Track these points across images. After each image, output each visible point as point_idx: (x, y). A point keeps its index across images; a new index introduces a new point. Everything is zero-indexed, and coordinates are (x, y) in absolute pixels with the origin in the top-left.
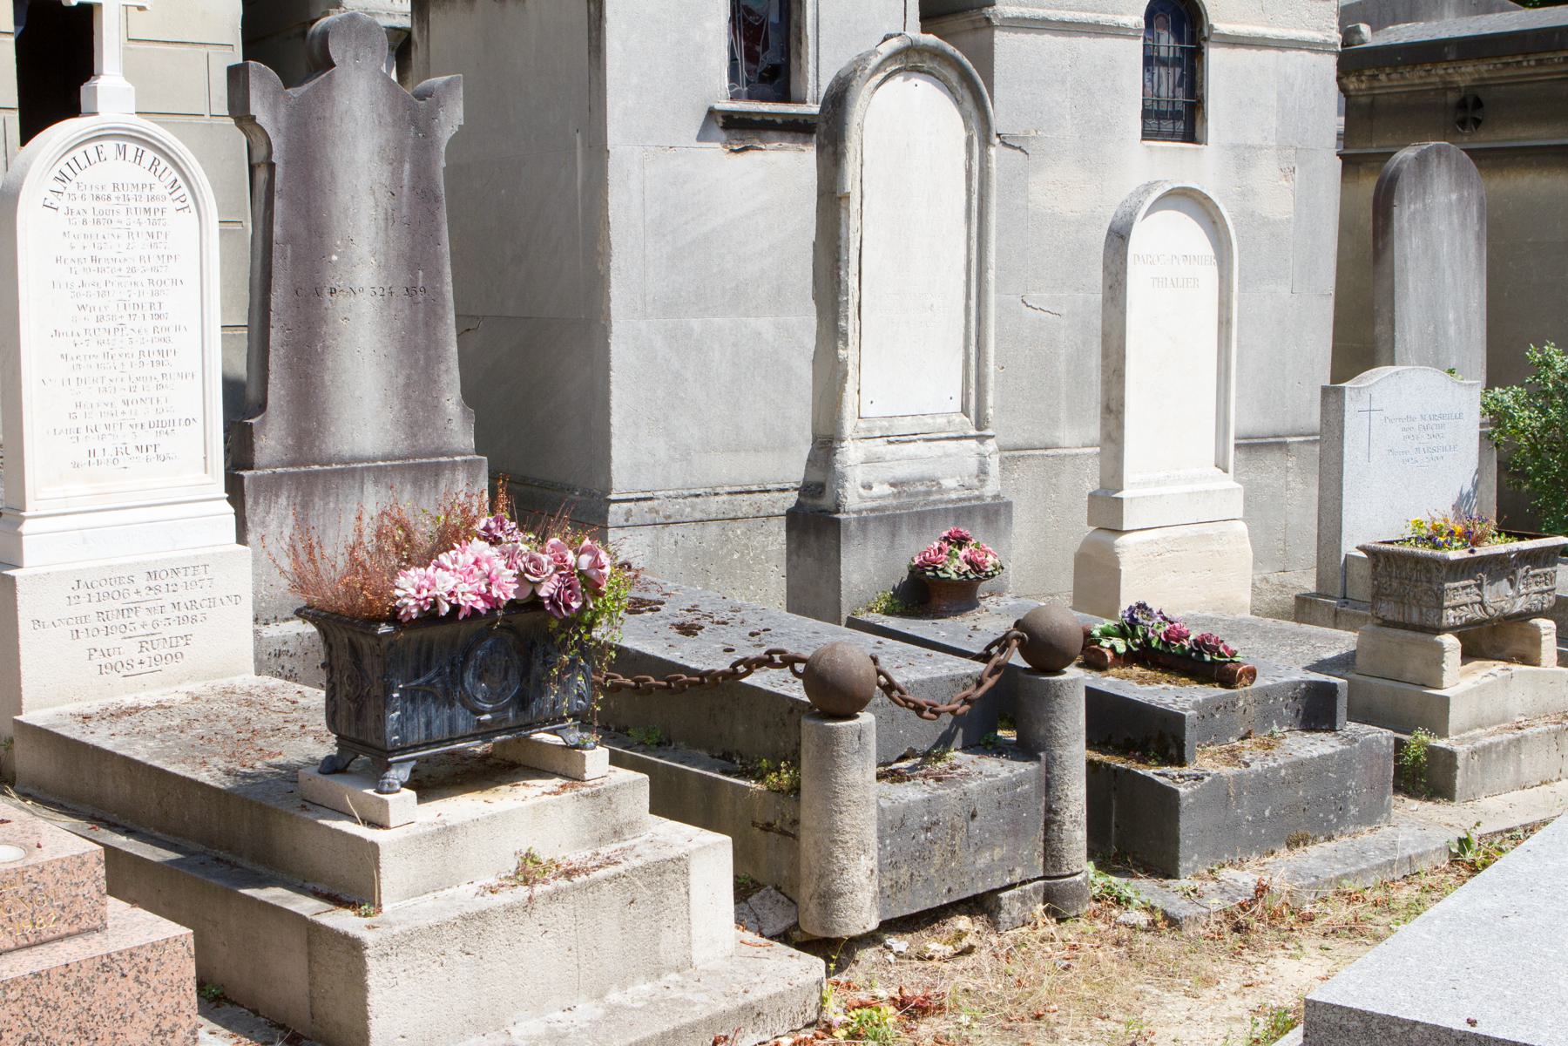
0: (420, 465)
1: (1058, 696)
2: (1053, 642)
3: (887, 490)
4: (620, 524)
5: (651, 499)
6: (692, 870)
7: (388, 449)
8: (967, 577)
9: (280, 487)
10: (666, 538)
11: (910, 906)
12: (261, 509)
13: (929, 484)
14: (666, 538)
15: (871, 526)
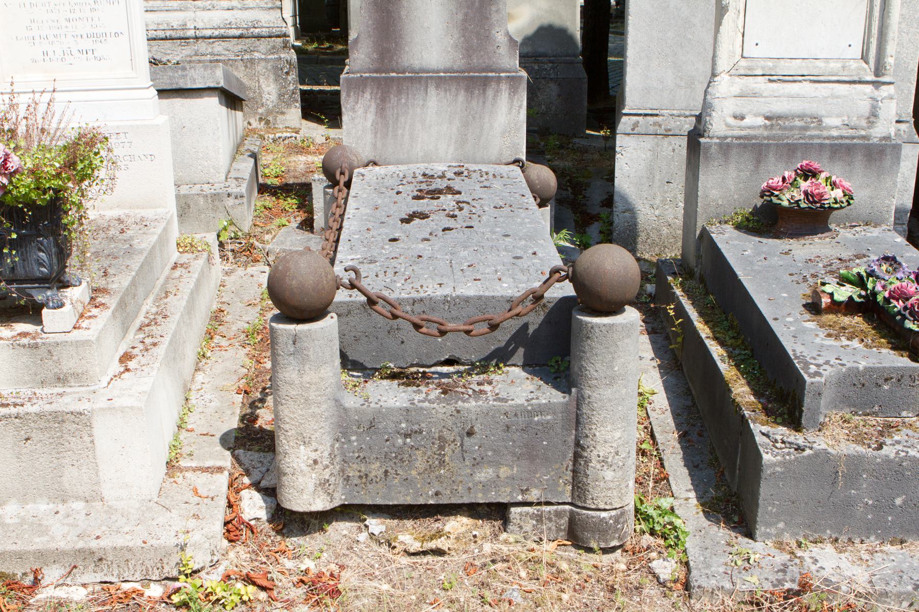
0: (472, 77)
1: (588, 338)
2: (586, 282)
3: (761, 121)
4: (627, 132)
5: (657, 115)
6: (95, 424)
7: (448, 65)
8: (798, 206)
9: (365, 87)
10: (665, 146)
11: (384, 497)
12: (351, 100)
13: (809, 120)
14: (665, 146)
15: (734, 151)
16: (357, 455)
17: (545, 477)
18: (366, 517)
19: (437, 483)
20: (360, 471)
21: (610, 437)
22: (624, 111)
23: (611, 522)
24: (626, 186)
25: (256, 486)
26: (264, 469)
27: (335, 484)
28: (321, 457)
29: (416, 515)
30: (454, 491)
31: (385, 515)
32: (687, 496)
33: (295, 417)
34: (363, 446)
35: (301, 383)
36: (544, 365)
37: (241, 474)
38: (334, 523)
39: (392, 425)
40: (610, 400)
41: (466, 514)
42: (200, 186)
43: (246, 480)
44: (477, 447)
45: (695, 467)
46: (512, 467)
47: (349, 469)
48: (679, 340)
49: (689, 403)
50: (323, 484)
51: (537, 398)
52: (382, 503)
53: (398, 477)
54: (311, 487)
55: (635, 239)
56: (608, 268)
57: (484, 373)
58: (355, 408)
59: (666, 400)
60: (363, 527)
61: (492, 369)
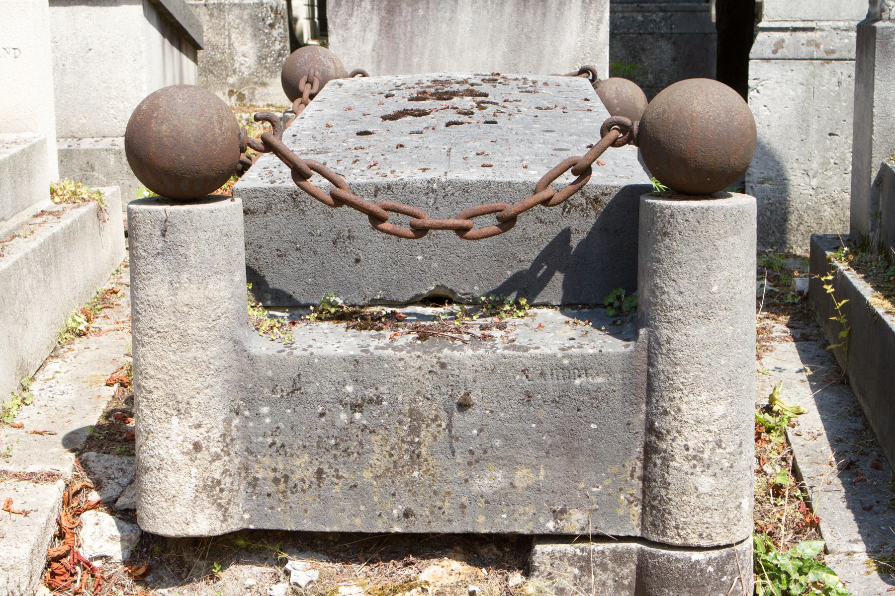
1: (666, 234)
2: (661, 136)
4: (766, 56)
5: (812, 29)
10: (826, 76)
11: (315, 519)
12: (343, 10)
14: (826, 76)
16: (270, 440)
17: (594, 489)
18: (285, 555)
19: (407, 494)
20: (275, 470)
21: (705, 413)
22: (760, 25)
23: (710, 569)
25: (110, 506)
26: (125, 481)
27: (231, 490)
28: (208, 439)
29: (375, 555)
30: (436, 511)
31: (320, 555)
32: (850, 549)
33: (164, 366)
34: (281, 424)
35: (174, 305)
36: (597, 305)
37: (87, 487)
38: (232, 567)
39: (329, 388)
40: (705, 346)
41: (458, 556)
42: (111, 139)
43: (94, 496)
44: (475, 432)
45: (865, 509)
46: (535, 469)
47: (256, 466)
48: (843, 334)
49: (859, 426)
50: (211, 487)
51: (580, 347)
52: (313, 528)
53: (341, 482)
54: (189, 492)
56: (699, 109)
57: (492, 315)
58: (268, 356)
59: (821, 422)
60: (283, 576)
61: (507, 308)
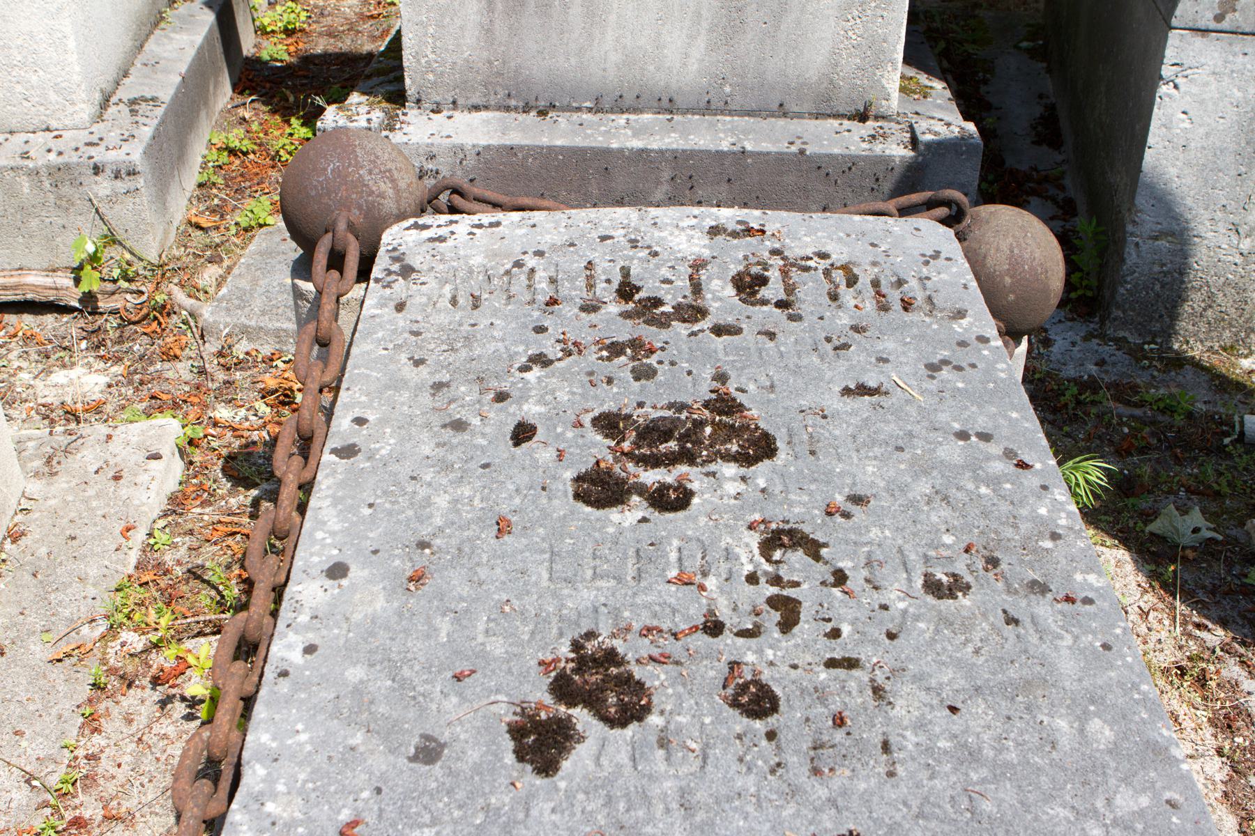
4: (1202, 24)
24: (1173, 171)
55: (1175, 307)
